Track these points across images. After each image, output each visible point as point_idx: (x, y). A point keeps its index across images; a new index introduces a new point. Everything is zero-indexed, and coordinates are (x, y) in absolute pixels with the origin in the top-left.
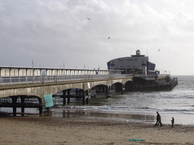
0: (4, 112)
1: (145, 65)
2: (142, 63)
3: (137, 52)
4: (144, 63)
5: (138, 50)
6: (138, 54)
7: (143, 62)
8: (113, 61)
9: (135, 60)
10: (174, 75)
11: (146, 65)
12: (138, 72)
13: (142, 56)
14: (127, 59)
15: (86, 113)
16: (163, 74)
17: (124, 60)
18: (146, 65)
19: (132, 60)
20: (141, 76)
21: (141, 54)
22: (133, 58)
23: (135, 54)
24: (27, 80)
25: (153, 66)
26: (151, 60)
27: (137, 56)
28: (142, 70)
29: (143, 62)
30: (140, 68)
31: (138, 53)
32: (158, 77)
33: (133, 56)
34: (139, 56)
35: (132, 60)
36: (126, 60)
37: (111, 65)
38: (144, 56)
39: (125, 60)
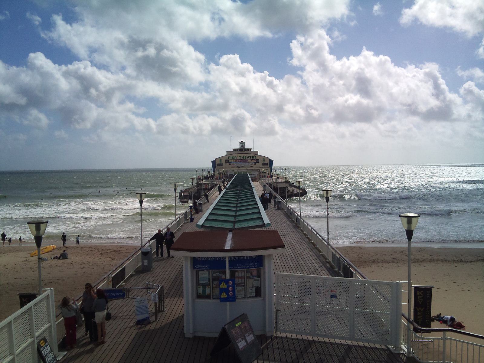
7: (264, 161)
8: (220, 159)
23: (238, 147)
29: (264, 161)
33: (235, 150)
36: (240, 157)
37: (219, 165)
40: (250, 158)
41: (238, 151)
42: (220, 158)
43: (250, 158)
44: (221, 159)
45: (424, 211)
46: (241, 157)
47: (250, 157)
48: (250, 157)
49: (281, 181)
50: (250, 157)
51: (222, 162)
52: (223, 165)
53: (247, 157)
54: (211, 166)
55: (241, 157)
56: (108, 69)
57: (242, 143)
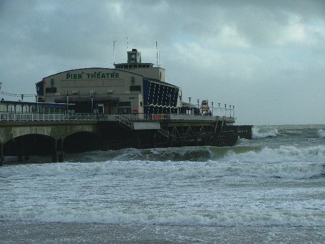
0: (104, 149)
3: (130, 54)
4: (136, 84)
5: (134, 50)
6: (132, 59)
7: (133, 81)
8: (52, 79)
10: (305, 123)
12: (119, 109)
14: (97, 74)
15: (255, 132)
17: (83, 76)
20: (122, 118)
23: (124, 60)
25: (173, 92)
26: (169, 79)
27: (131, 66)
28: (128, 104)
29: (133, 81)
30: (123, 99)
31: (133, 57)
33: (118, 66)
34: (135, 66)
36: (89, 75)
37: (48, 90)
39: (85, 77)
40: (108, 77)
41: (122, 67)
42: (52, 78)
43: (108, 77)
44: (52, 80)
45: (104, 221)
46: (90, 76)
47: (106, 76)
48: (108, 74)
49: (45, 128)
50: (106, 76)
51: (55, 86)
52: (57, 90)
53: (101, 75)
54: (34, 91)
55: (90, 76)
56: (183, 110)
57: (133, 54)
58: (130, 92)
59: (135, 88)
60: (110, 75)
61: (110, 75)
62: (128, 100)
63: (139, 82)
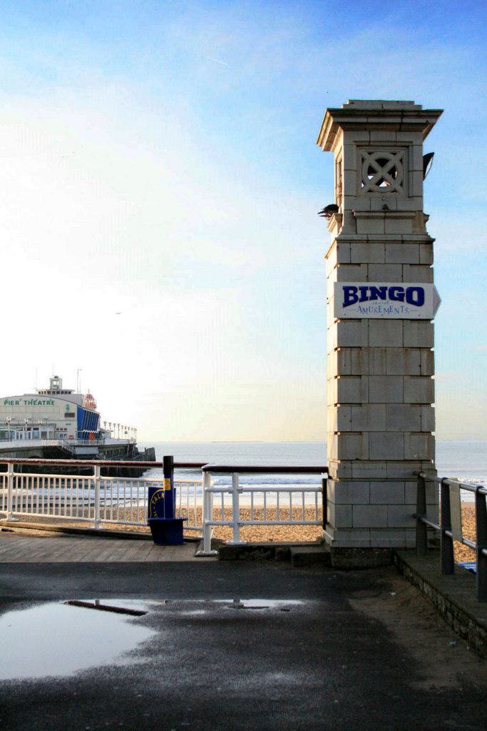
1: (72, 415)
2: (66, 411)
3: (52, 381)
5: (56, 377)
7: (68, 409)
9: (48, 403)
11: (169, 519)
13: (66, 393)
16: (417, 505)
18: (169, 519)
19: (40, 403)
21: (65, 387)
22: (41, 399)
23: (47, 387)
24: (11, 467)
27: (54, 393)
29: (68, 409)
31: (55, 383)
32: (454, 711)
34: (58, 393)
35: (40, 403)
36: (26, 402)
38: (70, 393)
39: (22, 403)
47: (42, 403)
50: (42, 403)
58: (64, 419)
59: (69, 415)
60: (46, 403)
61: (46, 403)
62: (65, 427)
63: (74, 410)
